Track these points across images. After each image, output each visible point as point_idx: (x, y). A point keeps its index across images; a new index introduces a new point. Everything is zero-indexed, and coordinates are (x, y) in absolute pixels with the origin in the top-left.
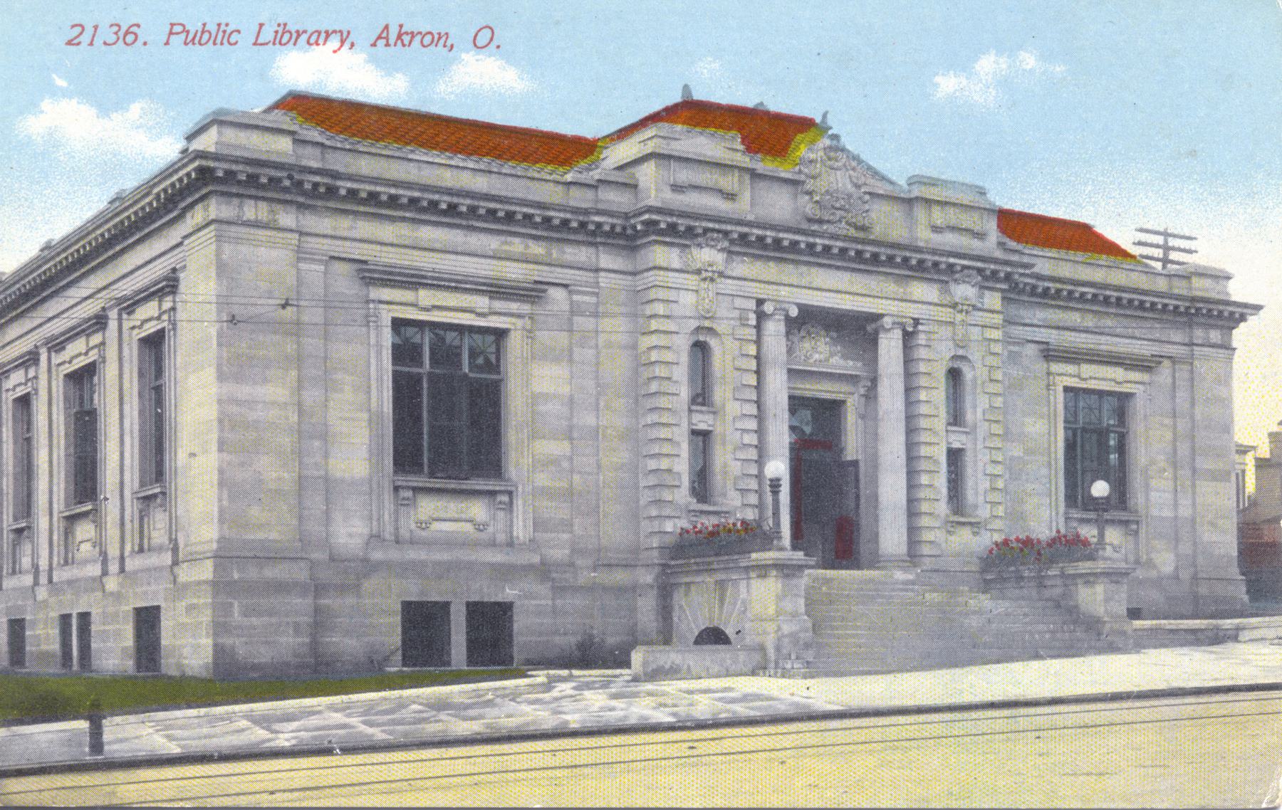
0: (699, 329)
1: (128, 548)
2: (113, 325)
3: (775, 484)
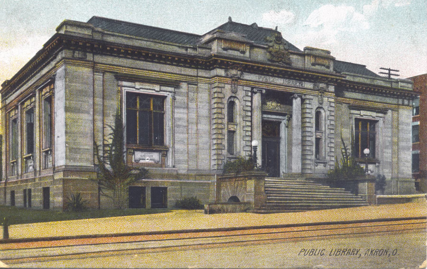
0: (231, 97)
1: (41, 168)
2: (37, 95)
3: (255, 148)
